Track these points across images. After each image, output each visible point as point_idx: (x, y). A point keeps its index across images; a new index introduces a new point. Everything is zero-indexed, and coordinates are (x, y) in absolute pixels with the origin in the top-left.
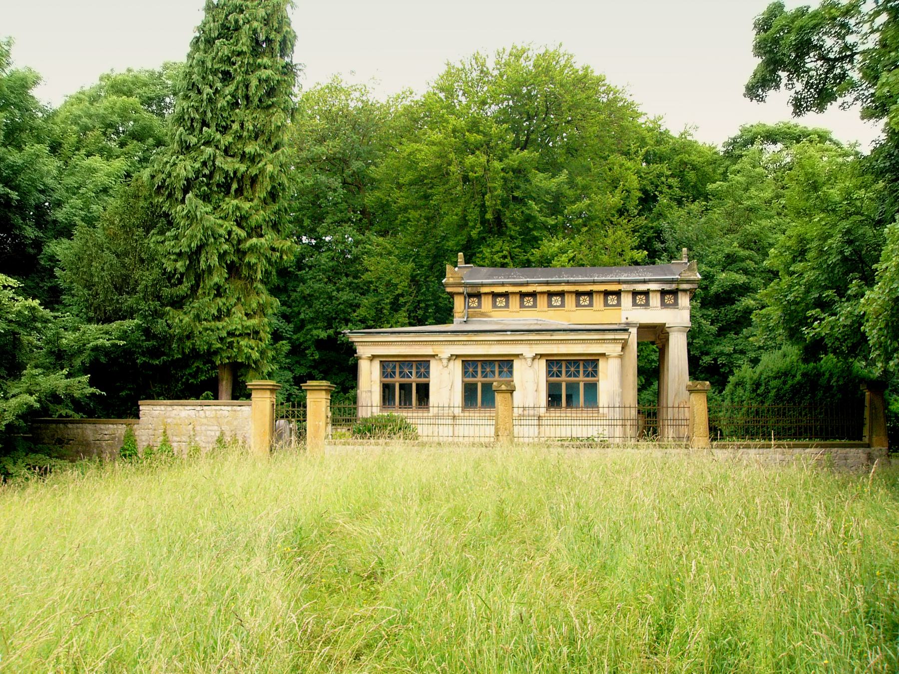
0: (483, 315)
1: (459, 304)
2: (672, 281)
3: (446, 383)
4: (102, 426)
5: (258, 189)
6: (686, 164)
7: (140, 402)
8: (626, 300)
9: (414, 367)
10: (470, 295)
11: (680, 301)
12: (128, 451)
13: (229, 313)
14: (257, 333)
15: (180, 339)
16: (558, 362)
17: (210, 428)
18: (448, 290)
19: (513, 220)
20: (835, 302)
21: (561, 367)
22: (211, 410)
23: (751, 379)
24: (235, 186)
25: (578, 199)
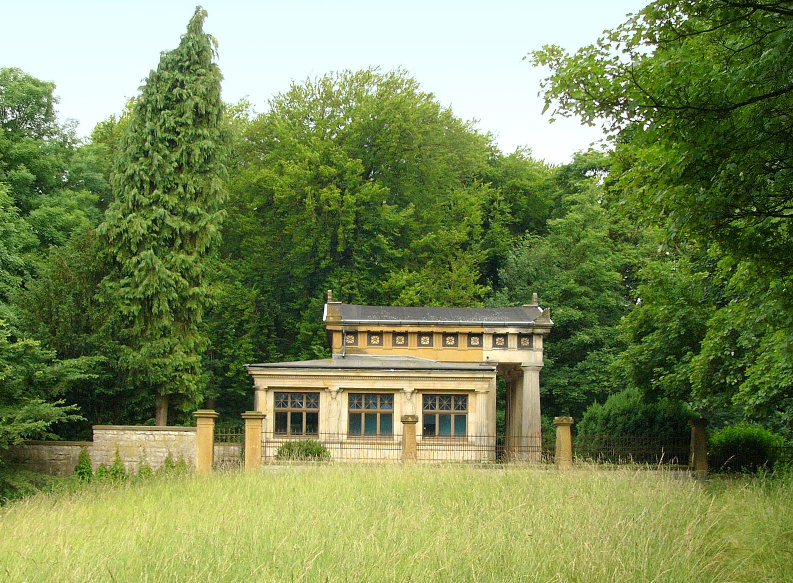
0: (359, 351)
1: (337, 339)
2: (528, 326)
3: (334, 414)
4: (58, 448)
5: (197, 244)
6: (518, 189)
7: (94, 427)
8: (488, 341)
9: (305, 398)
10: (348, 333)
11: (534, 344)
12: (82, 470)
13: (171, 351)
14: (192, 368)
15: (135, 373)
17: (159, 450)
18: (328, 328)
19: (361, 252)
20: (674, 364)
22: (160, 435)
23: (602, 415)
24: (179, 241)
25: (425, 231)
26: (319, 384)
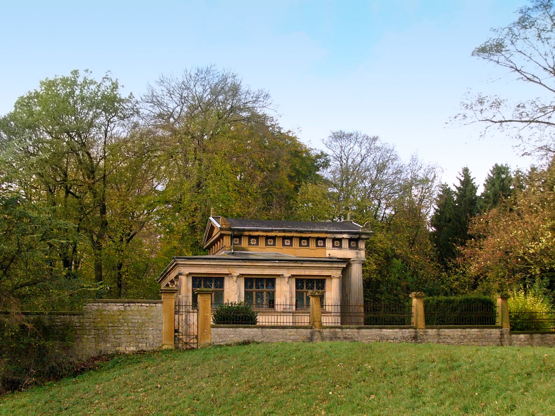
8: (329, 244)
11: (359, 245)
16: (302, 280)
21: (303, 283)
26: (226, 271)
